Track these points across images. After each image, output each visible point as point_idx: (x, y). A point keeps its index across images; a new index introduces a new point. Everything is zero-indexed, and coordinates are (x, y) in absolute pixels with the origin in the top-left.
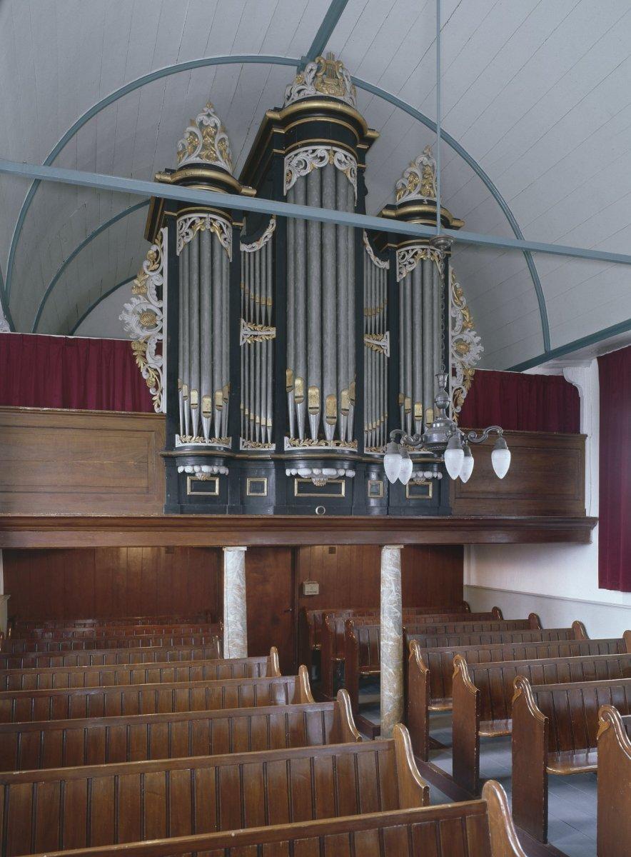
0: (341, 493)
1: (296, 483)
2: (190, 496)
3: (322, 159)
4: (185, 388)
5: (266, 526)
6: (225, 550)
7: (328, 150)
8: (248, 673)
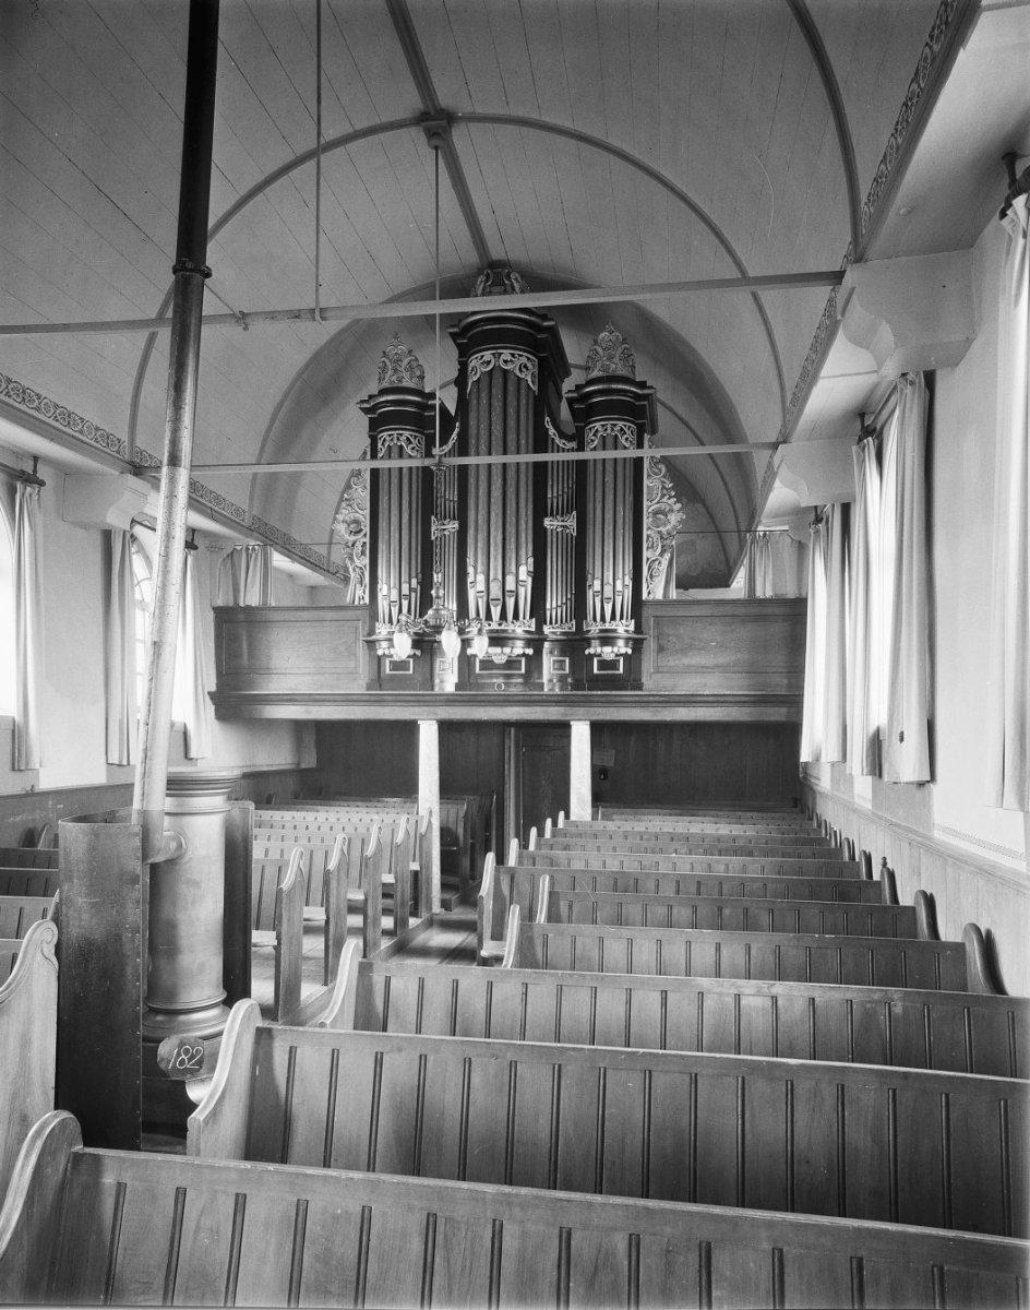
0: (520, 669)
1: (388, 662)
2: (597, 675)
3: (489, 362)
4: (385, 587)
5: (450, 700)
6: (572, 723)
7: (493, 354)
8: (591, 826)
